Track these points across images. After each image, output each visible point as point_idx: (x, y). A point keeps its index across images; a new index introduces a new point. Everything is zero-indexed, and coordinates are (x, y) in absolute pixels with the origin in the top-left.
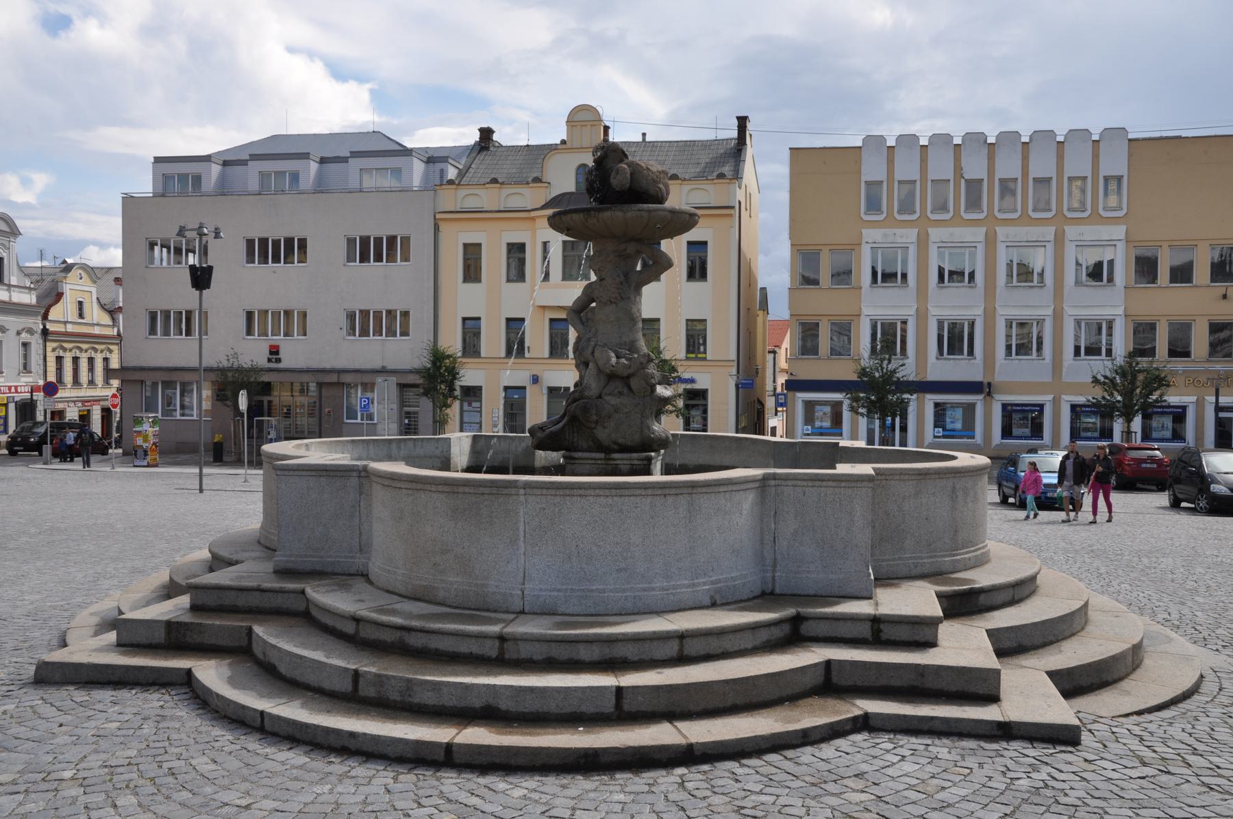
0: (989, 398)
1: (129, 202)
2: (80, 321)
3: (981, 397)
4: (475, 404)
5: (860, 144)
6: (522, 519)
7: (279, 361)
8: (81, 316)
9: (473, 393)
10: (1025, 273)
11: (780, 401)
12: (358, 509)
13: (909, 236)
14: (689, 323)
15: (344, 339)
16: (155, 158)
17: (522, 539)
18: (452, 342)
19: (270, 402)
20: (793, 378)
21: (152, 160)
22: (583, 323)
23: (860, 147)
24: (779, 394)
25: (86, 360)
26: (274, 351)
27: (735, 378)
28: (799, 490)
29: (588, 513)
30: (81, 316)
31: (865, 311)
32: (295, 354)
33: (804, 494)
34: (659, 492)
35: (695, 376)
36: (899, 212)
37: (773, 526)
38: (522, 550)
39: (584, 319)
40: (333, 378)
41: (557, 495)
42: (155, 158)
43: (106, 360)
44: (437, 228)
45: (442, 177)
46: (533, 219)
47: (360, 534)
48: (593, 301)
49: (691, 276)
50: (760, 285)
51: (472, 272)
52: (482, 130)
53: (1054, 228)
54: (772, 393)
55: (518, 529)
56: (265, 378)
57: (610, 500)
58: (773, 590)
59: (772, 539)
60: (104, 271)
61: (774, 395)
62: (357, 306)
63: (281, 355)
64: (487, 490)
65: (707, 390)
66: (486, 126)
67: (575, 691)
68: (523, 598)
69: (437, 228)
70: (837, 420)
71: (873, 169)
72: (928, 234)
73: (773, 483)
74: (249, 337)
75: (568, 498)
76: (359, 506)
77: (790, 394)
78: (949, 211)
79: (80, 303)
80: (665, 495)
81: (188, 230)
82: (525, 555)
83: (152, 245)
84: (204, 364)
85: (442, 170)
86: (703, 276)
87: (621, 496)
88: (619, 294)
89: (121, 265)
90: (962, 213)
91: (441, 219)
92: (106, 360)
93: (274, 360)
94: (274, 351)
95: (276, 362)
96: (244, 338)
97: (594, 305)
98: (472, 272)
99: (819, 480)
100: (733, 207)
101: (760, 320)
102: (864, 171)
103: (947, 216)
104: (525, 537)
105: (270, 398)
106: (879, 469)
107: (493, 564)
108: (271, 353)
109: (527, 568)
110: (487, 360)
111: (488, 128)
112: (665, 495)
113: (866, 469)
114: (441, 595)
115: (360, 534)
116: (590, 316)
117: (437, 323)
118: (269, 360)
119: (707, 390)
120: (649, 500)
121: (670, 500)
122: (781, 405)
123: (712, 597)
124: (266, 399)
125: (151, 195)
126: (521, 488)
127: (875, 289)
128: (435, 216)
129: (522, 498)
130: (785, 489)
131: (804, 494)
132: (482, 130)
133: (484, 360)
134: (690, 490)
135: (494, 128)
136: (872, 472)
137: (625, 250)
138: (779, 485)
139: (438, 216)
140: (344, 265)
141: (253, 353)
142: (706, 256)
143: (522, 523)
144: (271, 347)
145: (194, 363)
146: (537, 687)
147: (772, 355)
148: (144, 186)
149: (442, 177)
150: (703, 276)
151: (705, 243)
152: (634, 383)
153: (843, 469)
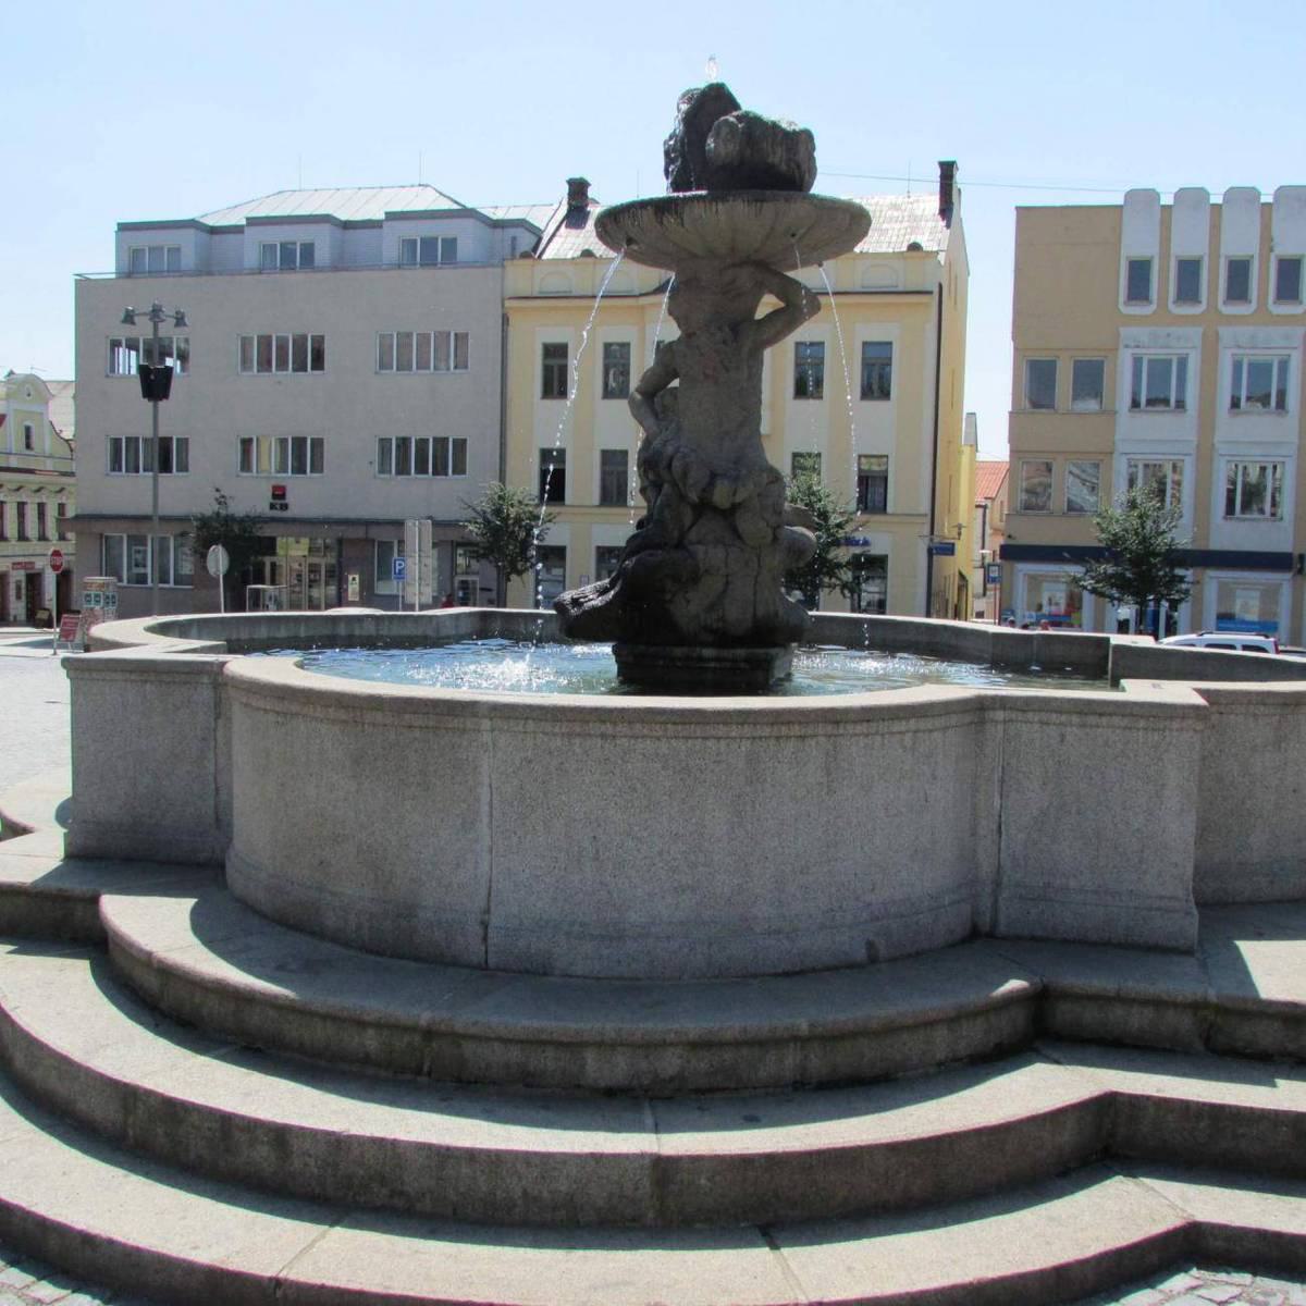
0: (1299, 577)
1: (86, 289)
2: (28, 452)
3: (1288, 576)
4: (557, 572)
5: (1119, 200)
6: (486, 781)
7: (285, 507)
8: (28, 446)
9: (554, 555)
10: (616, 804)
11: (992, 575)
12: (213, 744)
13: (1195, 334)
14: (863, 460)
15: (375, 477)
16: (119, 224)
17: (486, 820)
18: (525, 483)
19: (273, 565)
20: (1011, 542)
21: (116, 228)
22: (656, 415)
23: (1121, 206)
24: (989, 565)
25: (15, 505)
26: (279, 494)
27: (927, 540)
28: (1053, 731)
29: (617, 771)
30: (28, 446)
31: (1121, 447)
32: (307, 496)
33: (1062, 741)
34: (767, 731)
35: (869, 537)
36: (1174, 302)
37: (997, 802)
38: (487, 842)
39: (658, 407)
40: (360, 533)
41: (555, 735)
42: (119, 224)
43: (62, 507)
44: (505, 320)
45: (514, 248)
46: (643, 308)
47: (217, 789)
48: (675, 376)
49: (867, 392)
50: (966, 410)
51: (555, 383)
52: (571, 183)
53: (1201, 330)
54: (979, 564)
55: (478, 800)
56: (267, 531)
57: (664, 747)
58: (995, 923)
59: (995, 827)
60: (60, 387)
61: (983, 566)
62: (393, 435)
63: (290, 499)
64: (418, 721)
65: (886, 556)
66: (577, 176)
67: (565, 1162)
68: (485, 939)
69: (505, 320)
70: (1074, 604)
71: (1138, 242)
72: (1217, 334)
73: (1000, 715)
74: (245, 474)
75: (577, 741)
76: (215, 740)
77: (1007, 565)
78: (1200, 302)
79: (28, 429)
80: (778, 738)
81: (138, 315)
82: (491, 851)
83: (115, 344)
84: (161, 512)
85: (514, 239)
86: (885, 394)
87: (687, 738)
88: (722, 362)
89: (74, 379)
90: (1171, 306)
91: (511, 308)
92: (62, 507)
93: (278, 506)
94: (279, 494)
95: (281, 508)
96: (238, 476)
97: (675, 383)
98: (555, 383)
99: (1094, 713)
100: (930, 293)
101: (965, 460)
102: (1126, 240)
103: (1148, 310)
104: (491, 816)
105: (274, 559)
106: (1217, 692)
107: (430, 867)
108: (275, 496)
109: (494, 879)
110: (576, 510)
111: (581, 179)
112: (778, 738)
113: (1182, 692)
114: (331, 921)
115: (217, 789)
116: (668, 400)
117: (505, 453)
118: (272, 507)
119: (886, 556)
120: (746, 745)
121: (791, 746)
122: (994, 580)
123: (870, 945)
124: (268, 560)
125: (113, 276)
126: (485, 717)
127: (1138, 415)
128: (503, 306)
129: (486, 737)
130: (1024, 727)
131: (1062, 741)
132: (571, 183)
133: (895, 519)
134: (830, 729)
135: (589, 179)
136: (1200, 701)
137: (733, 281)
138: (1011, 721)
139: (508, 304)
140: (376, 373)
141: (249, 498)
142: (629, 364)
143: (486, 789)
144: (275, 488)
145: (147, 510)
146: (481, 1151)
147: (981, 511)
148: (104, 264)
149: (514, 248)
150: (885, 394)
151: (823, 343)
152: (745, 524)
153: (1137, 690)
